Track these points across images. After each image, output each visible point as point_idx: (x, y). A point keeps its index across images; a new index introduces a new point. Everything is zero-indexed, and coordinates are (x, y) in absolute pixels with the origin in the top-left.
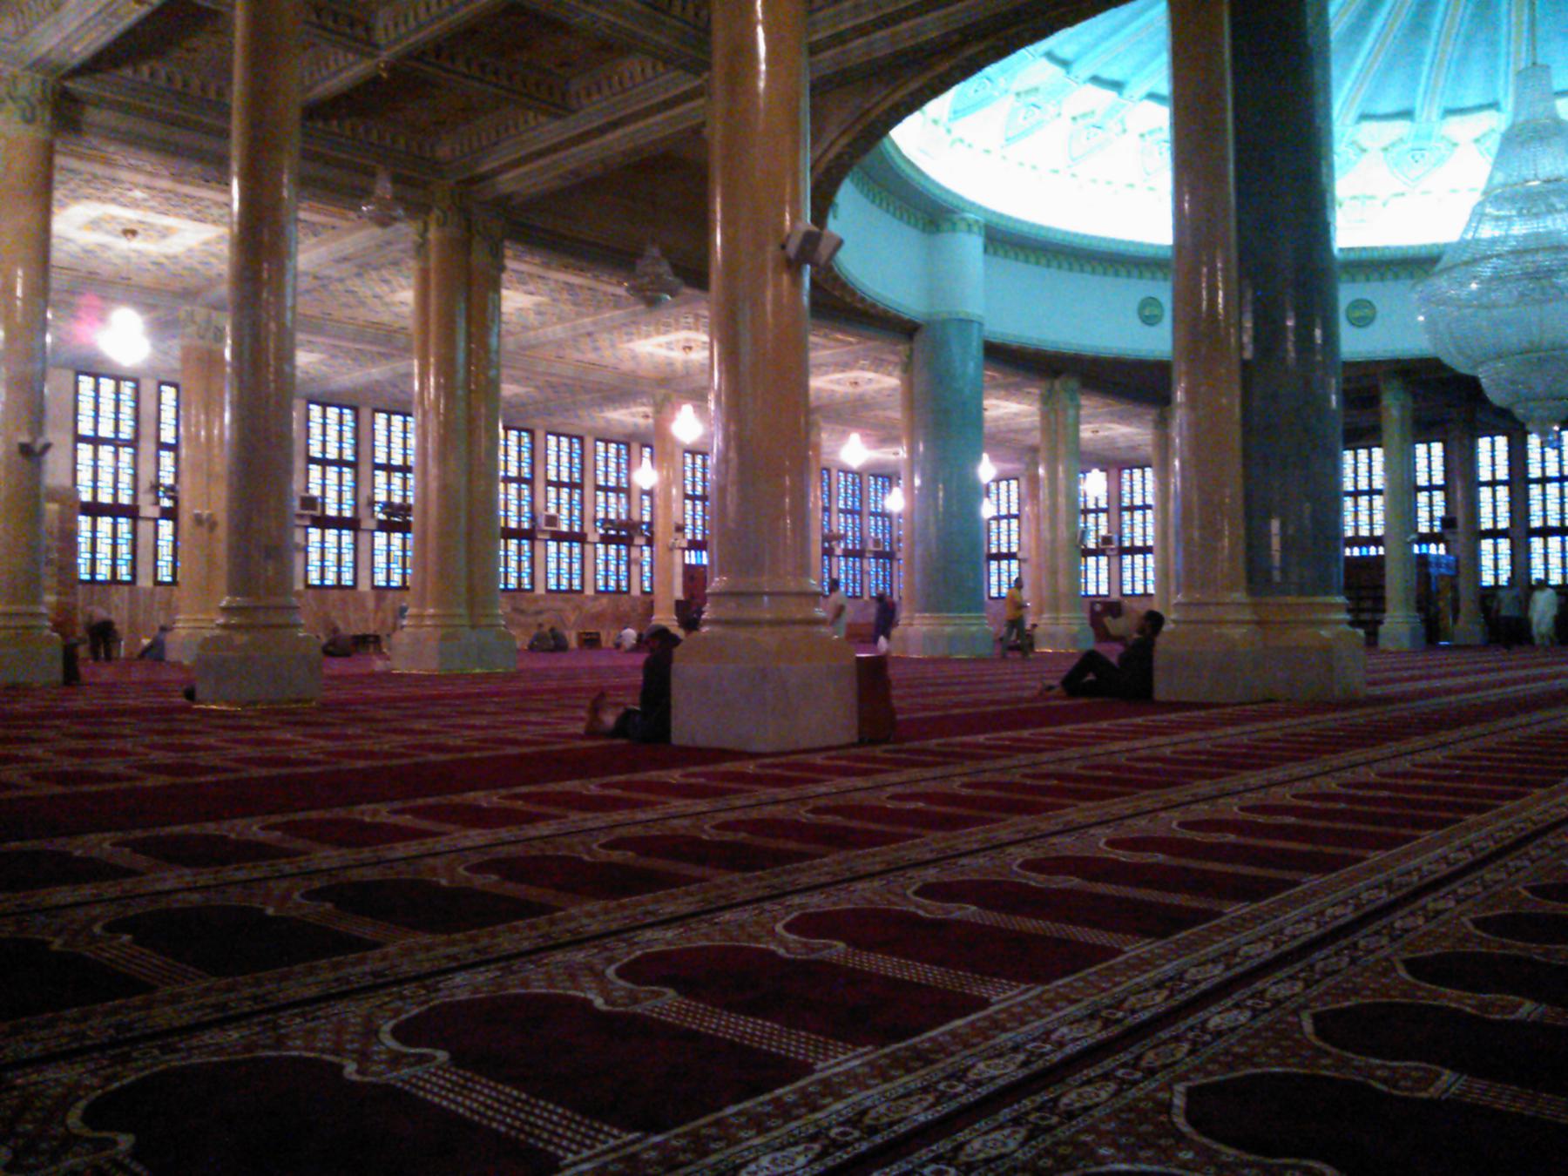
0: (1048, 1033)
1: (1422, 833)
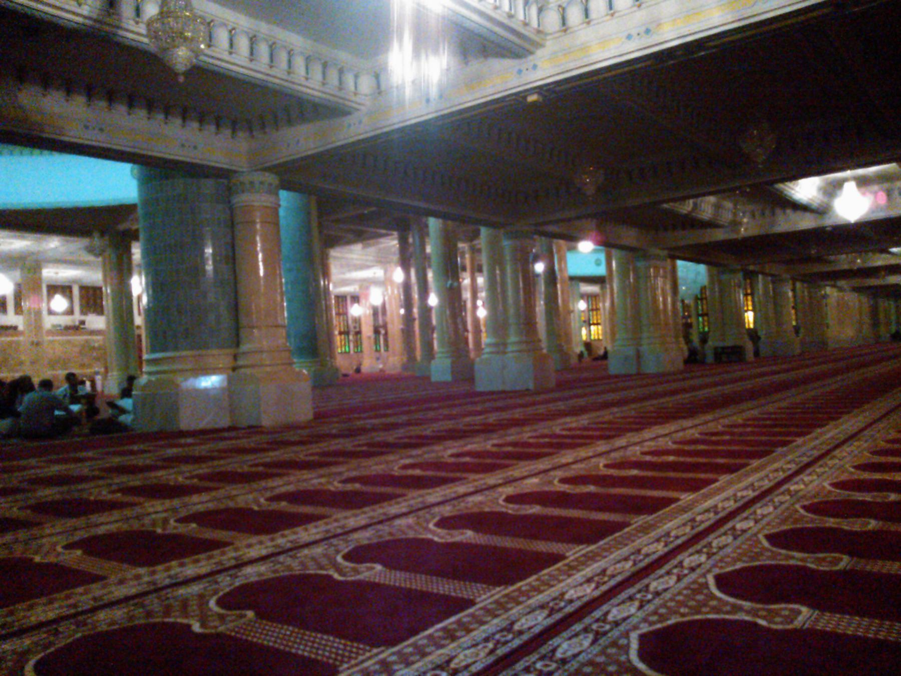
0: (563, 594)
1: (751, 461)
